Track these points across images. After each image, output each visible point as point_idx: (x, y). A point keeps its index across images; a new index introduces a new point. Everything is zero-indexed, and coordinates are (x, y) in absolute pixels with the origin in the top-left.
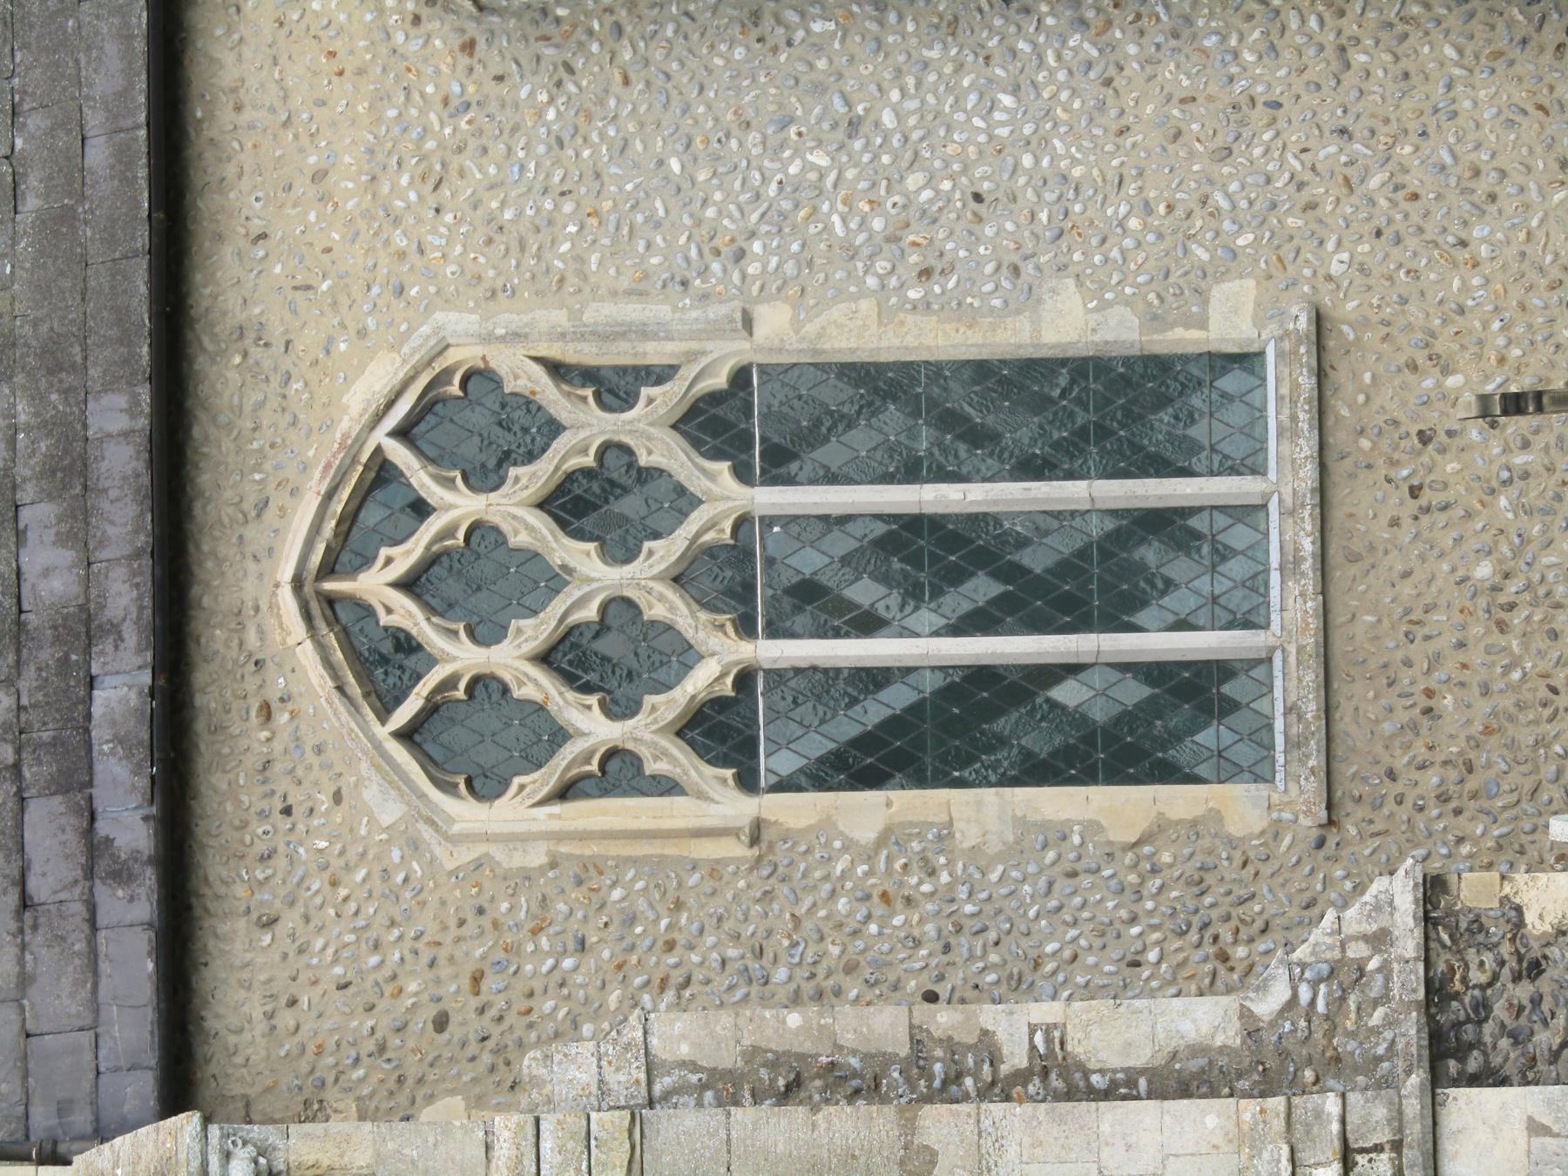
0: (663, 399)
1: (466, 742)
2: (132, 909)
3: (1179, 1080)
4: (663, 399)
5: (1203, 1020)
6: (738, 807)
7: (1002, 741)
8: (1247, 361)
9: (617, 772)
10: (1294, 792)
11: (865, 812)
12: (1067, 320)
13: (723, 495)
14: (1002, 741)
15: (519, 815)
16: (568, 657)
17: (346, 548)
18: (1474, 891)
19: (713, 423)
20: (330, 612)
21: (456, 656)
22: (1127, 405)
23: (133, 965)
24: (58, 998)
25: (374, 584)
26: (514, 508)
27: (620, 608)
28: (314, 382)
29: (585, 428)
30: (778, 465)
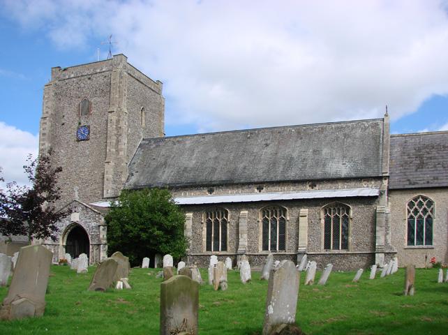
0: (430, 214)
1: (411, 205)
2: (402, 187)
3: (386, 240)
4: (430, 214)
5: (389, 241)
6: (407, 218)
7: (15, 208)
8: (432, 244)
9: (409, 212)
10: (406, 246)
11: (406, 225)
12: (434, 235)
13: (425, 217)
14: (15, 208)
15: (407, 207)
16: (416, 209)
17: (423, 197)
18: (396, 255)
19: (429, 216)
20: (418, 197)
21: (416, 203)
22: (430, 240)
23: (398, 187)
24: (422, 182)
25: (421, 199)
26: (425, 206)
27: (422, 212)
28: (431, 196)
29: (429, 210)
30: (427, 220)
